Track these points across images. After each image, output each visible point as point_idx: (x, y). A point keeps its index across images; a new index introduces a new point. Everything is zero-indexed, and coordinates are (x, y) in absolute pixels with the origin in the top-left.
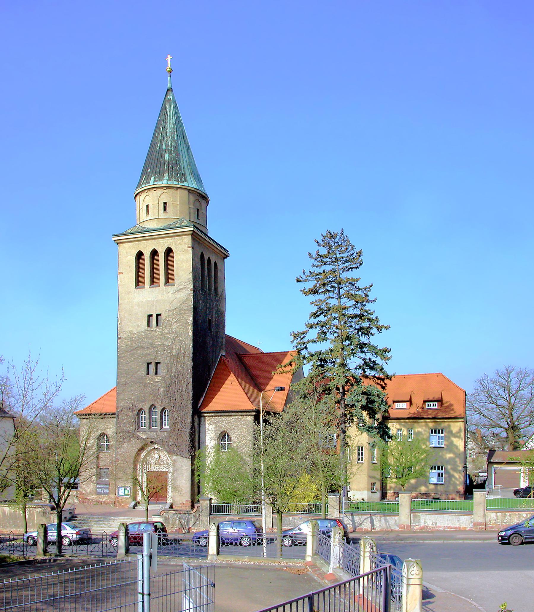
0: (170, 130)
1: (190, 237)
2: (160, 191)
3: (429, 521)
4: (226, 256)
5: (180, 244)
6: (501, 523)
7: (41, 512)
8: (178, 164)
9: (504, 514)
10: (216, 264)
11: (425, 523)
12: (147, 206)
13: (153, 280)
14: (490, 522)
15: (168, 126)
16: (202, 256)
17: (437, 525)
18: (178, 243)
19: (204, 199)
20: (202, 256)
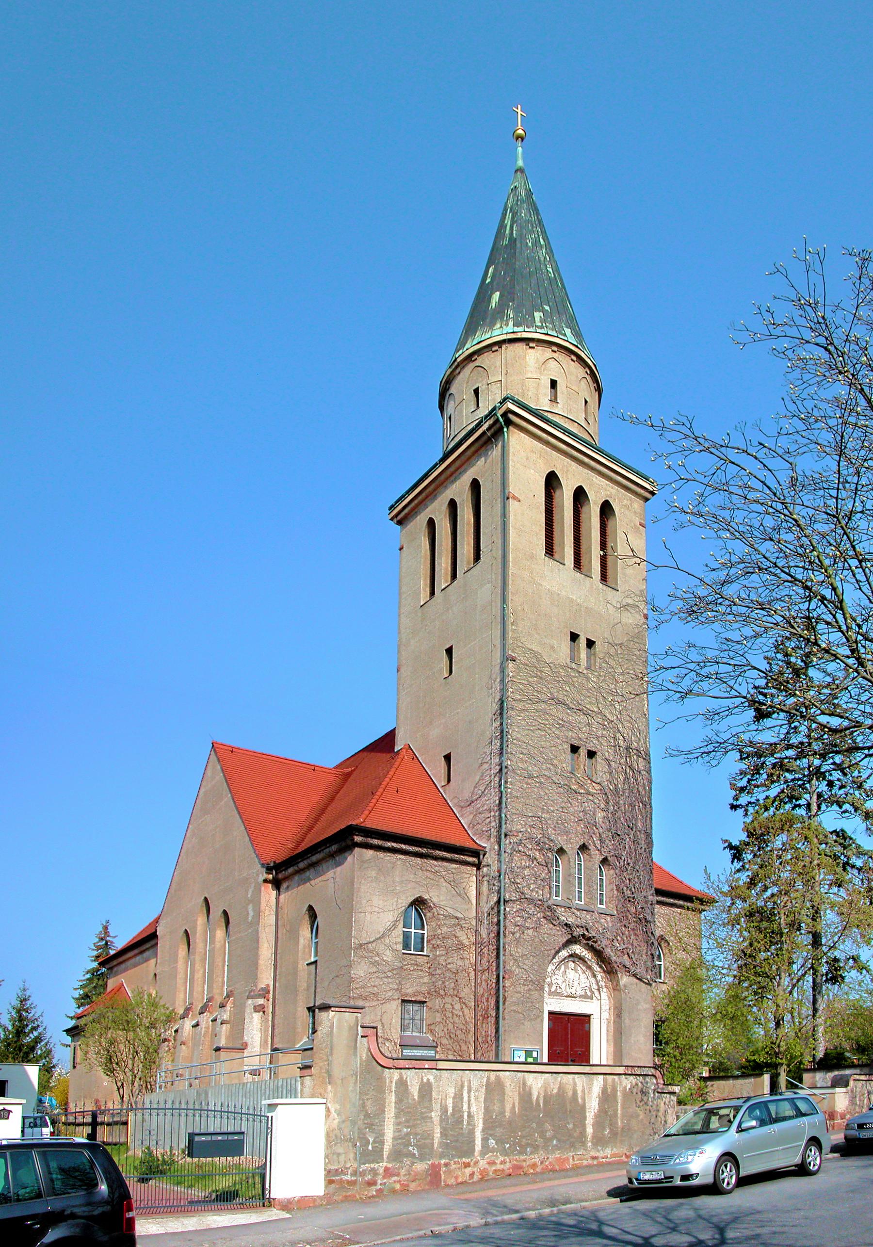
7: (635, 1090)
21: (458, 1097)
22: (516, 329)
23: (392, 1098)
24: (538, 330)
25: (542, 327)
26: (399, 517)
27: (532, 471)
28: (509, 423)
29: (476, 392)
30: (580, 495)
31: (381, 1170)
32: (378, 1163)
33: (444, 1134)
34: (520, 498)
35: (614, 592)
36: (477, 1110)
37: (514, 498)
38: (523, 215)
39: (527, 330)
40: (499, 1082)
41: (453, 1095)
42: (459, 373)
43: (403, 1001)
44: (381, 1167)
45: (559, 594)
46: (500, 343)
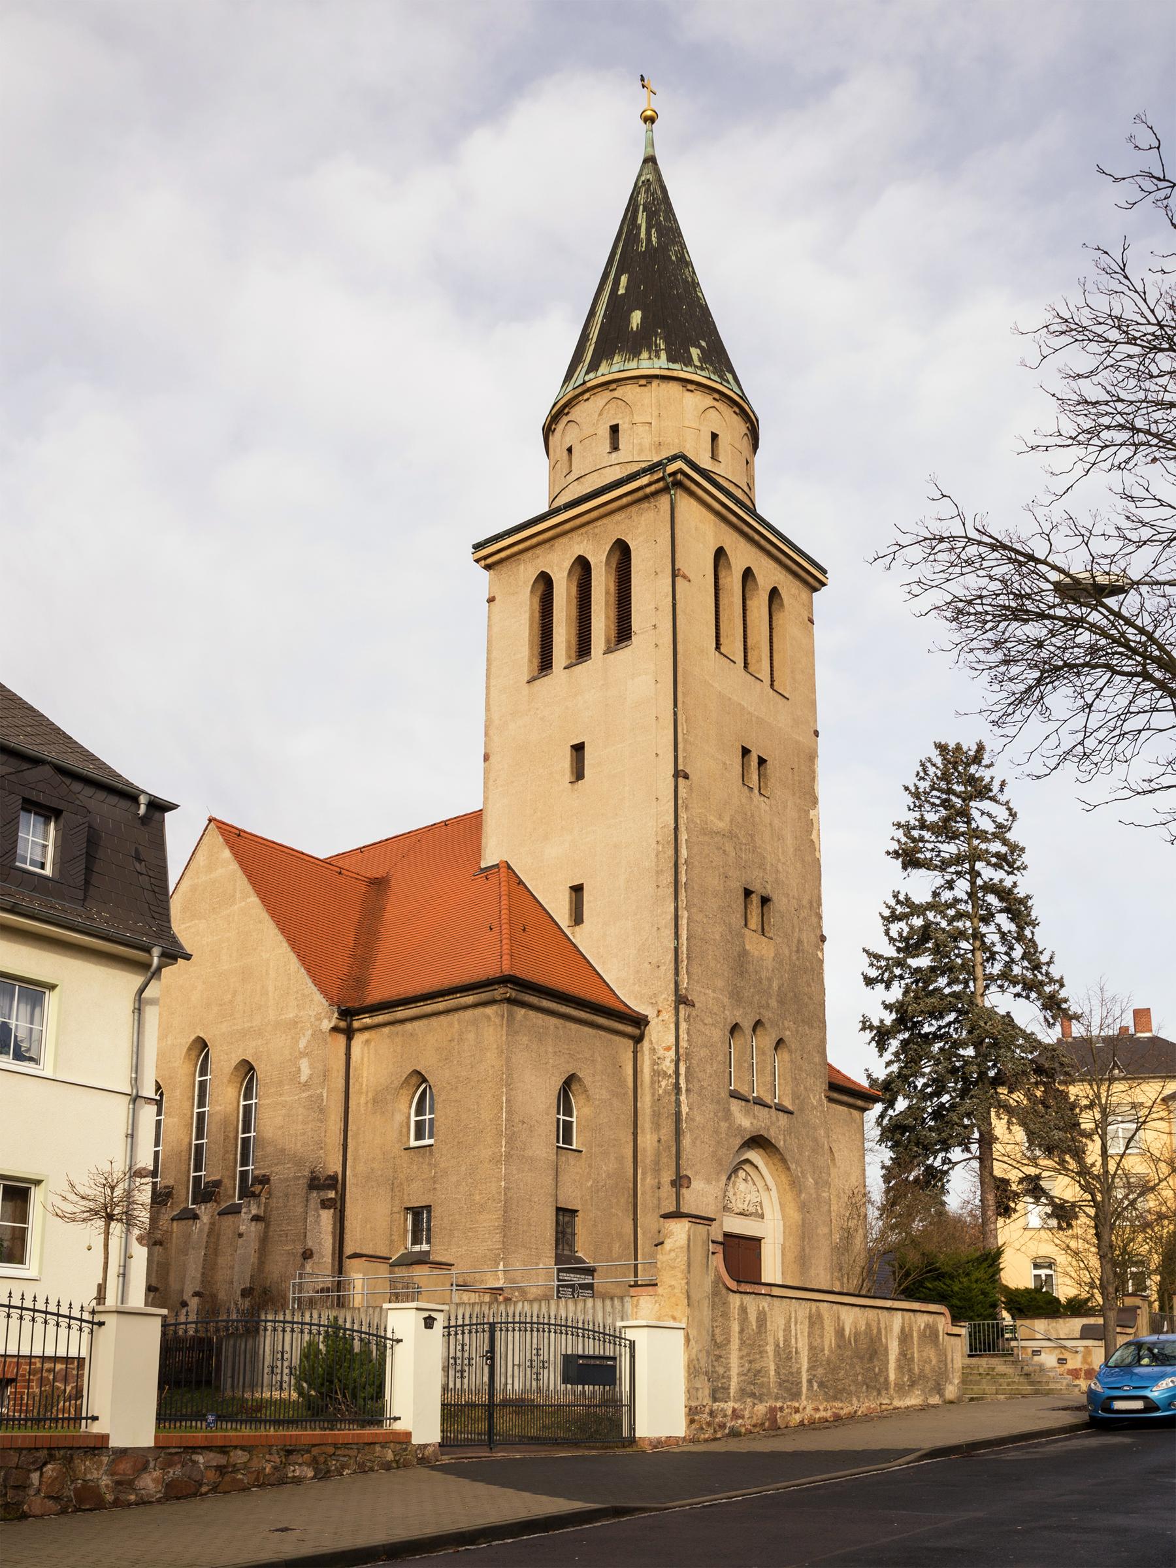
13: (583, 649)
21: (787, 1329)
22: (671, 366)
23: (735, 1327)
24: (699, 372)
25: (702, 369)
26: (489, 561)
27: (701, 545)
28: (678, 484)
29: (615, 429)
30: (748, 574)
31: (729, 1412)
32: (726, 1402)
33: (777, 1373)
34: (691, 578)
35: (785, 700)
36: (802, 1345)
37: (684, 577)
38: (662, 219)
39: (685, 369)
40: (819, 1316)
41: (783, 1327)
42: (588, 399)
43: (559, 1209)
44: (729, 1406)
45: (730, 699)
46: (650, 378)
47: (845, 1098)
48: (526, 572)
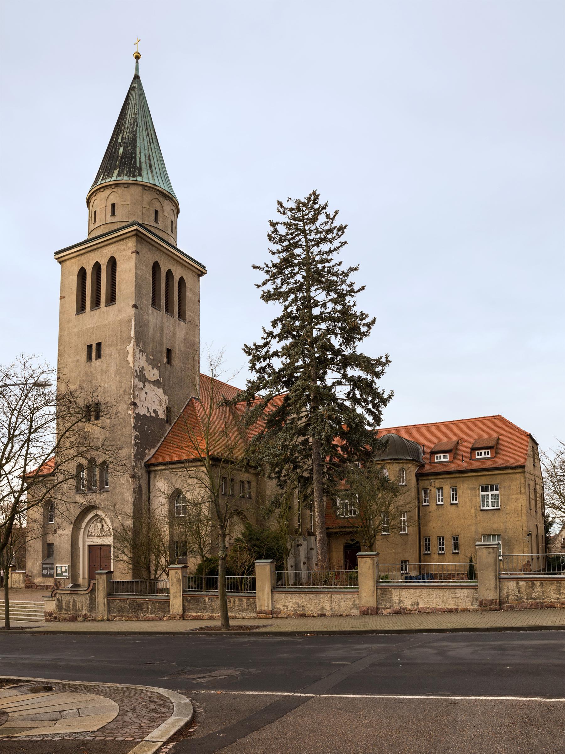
0: (130, 121)
1: (134, 239)
2: (108, 191)
3: (405, 599)
4: (202, 274)
5: (124, 250)
6: (527, 599)
8: (134, 157)
9: (530, 583)
10: (182, 281)
11: (399, 604)
12: (95, 212)
13: (96, 303)
14: (508, 598)
15: (128, 117)
16: (156, 267)
17: (420, 606)
18: (122, 249)
19: (167, 200)
20: (156, 267)
47: (448, 476)
48: (74, 267)
